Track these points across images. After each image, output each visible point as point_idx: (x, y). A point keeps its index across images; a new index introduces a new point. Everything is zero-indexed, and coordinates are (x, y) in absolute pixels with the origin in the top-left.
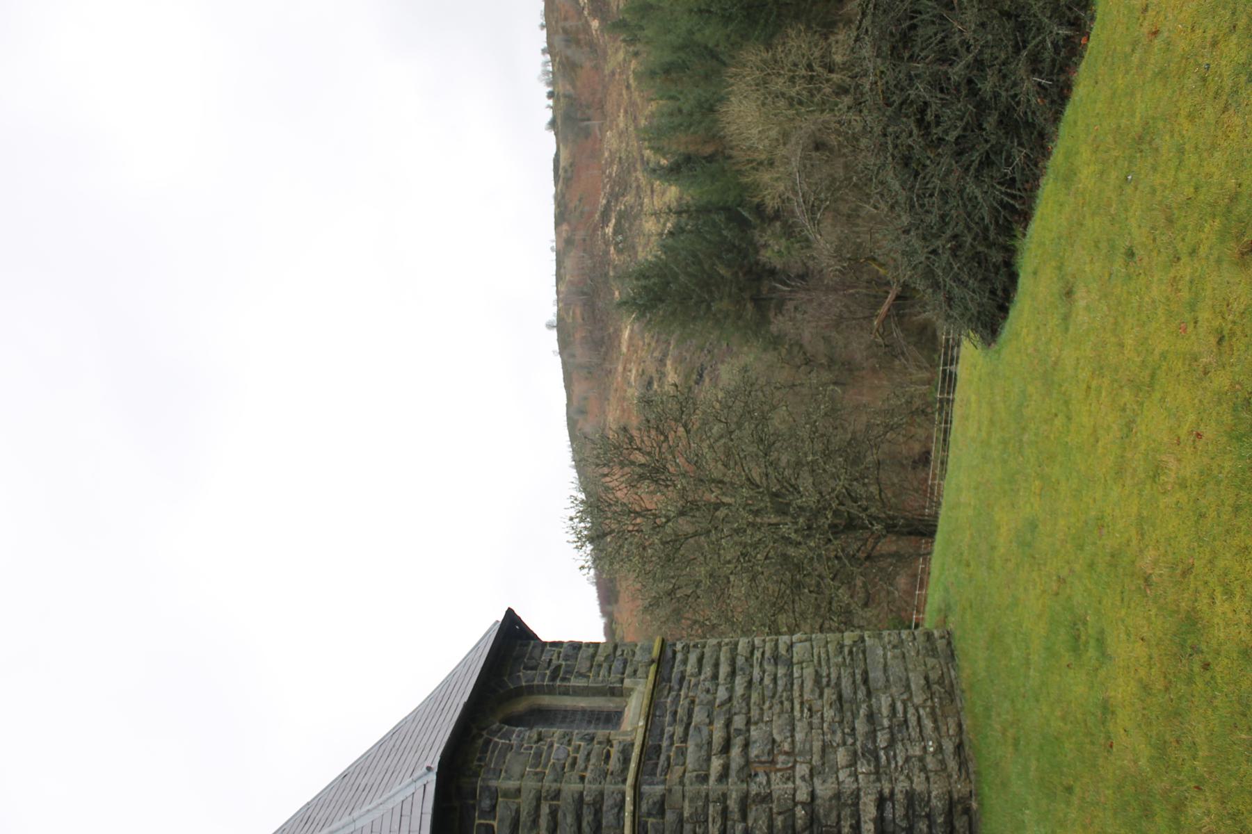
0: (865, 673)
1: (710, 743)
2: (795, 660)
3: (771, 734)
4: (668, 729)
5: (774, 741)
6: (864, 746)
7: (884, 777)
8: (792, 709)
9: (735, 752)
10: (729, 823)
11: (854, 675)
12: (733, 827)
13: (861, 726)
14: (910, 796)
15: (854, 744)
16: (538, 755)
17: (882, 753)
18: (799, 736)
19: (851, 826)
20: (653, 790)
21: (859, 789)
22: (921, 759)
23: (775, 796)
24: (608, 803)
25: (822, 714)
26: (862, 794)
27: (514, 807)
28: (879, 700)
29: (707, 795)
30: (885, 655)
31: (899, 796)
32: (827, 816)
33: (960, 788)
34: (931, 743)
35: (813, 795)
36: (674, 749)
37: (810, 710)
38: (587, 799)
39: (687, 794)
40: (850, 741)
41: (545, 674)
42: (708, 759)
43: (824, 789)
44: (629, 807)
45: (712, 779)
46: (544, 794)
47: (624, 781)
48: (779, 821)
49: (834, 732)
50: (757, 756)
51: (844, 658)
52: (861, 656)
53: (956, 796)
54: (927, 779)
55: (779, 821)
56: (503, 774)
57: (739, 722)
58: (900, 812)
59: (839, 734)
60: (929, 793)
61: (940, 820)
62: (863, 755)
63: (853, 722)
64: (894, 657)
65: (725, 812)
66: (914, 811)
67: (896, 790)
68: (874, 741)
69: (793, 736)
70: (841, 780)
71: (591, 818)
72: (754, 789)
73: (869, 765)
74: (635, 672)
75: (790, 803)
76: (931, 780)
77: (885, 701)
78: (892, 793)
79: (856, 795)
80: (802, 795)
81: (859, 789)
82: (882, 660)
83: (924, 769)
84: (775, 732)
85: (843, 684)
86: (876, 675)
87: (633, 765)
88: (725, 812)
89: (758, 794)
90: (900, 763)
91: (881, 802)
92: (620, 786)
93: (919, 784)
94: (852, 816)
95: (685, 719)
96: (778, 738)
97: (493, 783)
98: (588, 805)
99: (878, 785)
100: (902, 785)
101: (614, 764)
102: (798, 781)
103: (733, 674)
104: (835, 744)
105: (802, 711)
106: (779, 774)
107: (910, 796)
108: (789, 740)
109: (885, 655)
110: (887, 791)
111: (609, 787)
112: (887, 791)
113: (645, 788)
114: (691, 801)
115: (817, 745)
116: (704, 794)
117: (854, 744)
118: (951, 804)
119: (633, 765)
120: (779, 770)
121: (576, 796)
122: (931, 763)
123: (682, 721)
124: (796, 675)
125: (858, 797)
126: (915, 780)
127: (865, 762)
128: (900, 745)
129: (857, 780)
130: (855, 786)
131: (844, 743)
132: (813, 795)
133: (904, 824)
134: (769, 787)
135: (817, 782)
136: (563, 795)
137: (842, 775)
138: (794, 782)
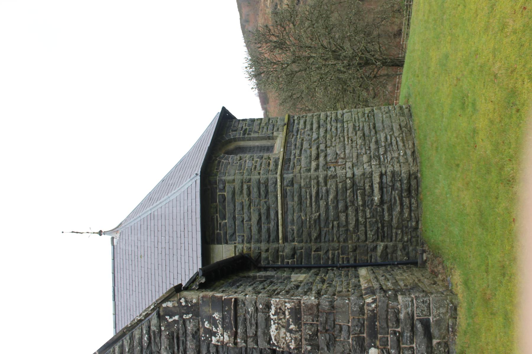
0: (374, 124)
1: (311, 156)
2: (345, 120)
3: (336, 151)
4: (293, 152)
5: (337, 154)
6: (374, 154)
7: (382, 166)
8: (344, 140)
9: (321, 159)
10: (320, 187)
11: (369, 125)
12: (322, 189)
13: (373, 146)
14: (393, 173)
15: (370, 153)
16: (241, 165)
17: (381, 156)
18: (347, 151)
19: (369, 186)
20: (288, 176)
21: (372, 171)
22: (398, 158)
23: (338, 175)
24: (270, 182)
25: (357, 142)
26: (373, 173)
27: (232, 187)
28: (380, 135)
29: (310, 177)
30: (382, 117)
31: (389, 173)
32: (359, 182)
33: (413, 169)
34: (402, 152)
35: (354, 174)
36: (296, 159)
37: (351, 140)
38: (262, 181)
39: (302, 177)
40: (368, 152)
41: (241, 133)
42: (310, 162)
43: (358, 172)
44: (279, 184)
45: (312, 170)
46: (244, 181)
47: (276, 173)
48: (340, 185)
49: (362, 149)
50: (330, 160)
51: (365, 118)
52: (372, 117)
53: (412, 172)
54: (400, 166)
55: (340, 185)
56: (227, 174)
57: (322, 147)
58: (389, 179)
59: (364, 150)
60: (401, 171)
61: (405, 182)
62: (374, 157)
63: (370, 144)
64: (386, 117)
65: (318, 183)
66: (395, 179)
67: (388, 171)
68: (378, 152)
69: (345, 151)
70: (365, 168)
71: (264, 189)
72: (329, 173)
73: (376, 161)
74: (278, 129)
75: (344, 178)
76: (402, 166)
77: (382, 136)
78: (386, 172)
79: (371, 173)
80: (349, 175)
81: (372, 171)
82: (381, 119)
83: (399, 162)
84: (337, 150)
85: (365, 129)
86: (379, 125)
88: (318, 183)
89: (331, 175)
90: (389, 160)
91: (381, 176)
92: (275, 175)
93: (397, 168)
94: (370, 182)
95: (300, 147)
96: (338, 152)
97: (223, 178)
98: (263, 184)
99: (380, 169)
100: (390, 169)
101: (272, 167)
102: (347, 169)
103: (319, 127)
104: (362, 154)
105: (348, 141)
106: (340, 167)
107: (393, 173)
108: (343, 153)
109: (382, 117)
110: (383, 172)
111: (270, 176)
112: (383, 172)
113: (285, 176)
114: (304, 179)
115: (355, 155)
116: (309, 176)
117: (370, 153)
118: (410, 175)
120: (340, 165)
121: (257, 180)
122: (402, 159)
123: (299, 148)
124: (345, 126)
125: (372, 174)
126: (395, 166)
127: (375, 160)
128: (389, 153)
129: (371, 167)
130: (370, 170)
131: (366, 153)
132: (354, 174)
133: (391, 184)
134: (336, 172)
135: (355, 169)
136: (252, 180)
137: (365, 166)
138: (346, 170)
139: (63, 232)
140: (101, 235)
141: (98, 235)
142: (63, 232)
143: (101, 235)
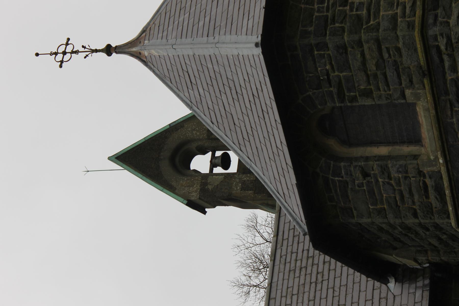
87: (447, 192)
119: (447, 192)
139: (37, 55)
140: (109, 54)
141: (104, 55)
142: (37, 55)
143: (109, 54)
